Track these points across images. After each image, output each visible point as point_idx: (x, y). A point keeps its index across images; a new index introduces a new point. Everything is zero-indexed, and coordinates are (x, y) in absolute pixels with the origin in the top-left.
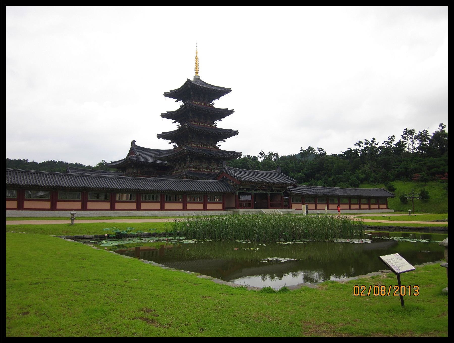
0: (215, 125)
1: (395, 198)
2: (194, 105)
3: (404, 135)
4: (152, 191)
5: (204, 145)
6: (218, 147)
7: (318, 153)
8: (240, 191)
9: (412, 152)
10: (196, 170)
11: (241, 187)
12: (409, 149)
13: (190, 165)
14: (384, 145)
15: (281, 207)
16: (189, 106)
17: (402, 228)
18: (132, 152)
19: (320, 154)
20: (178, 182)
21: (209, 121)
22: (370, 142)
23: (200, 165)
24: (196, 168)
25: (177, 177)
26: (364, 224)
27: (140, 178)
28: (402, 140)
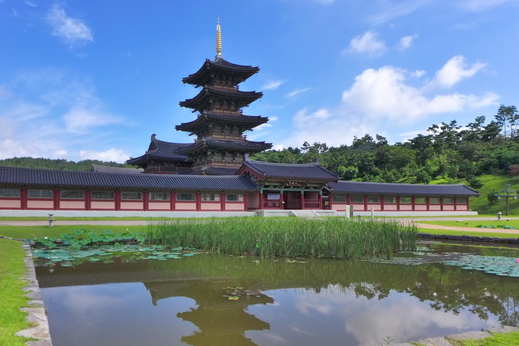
1: (480, 197)
3: (499, 114)
5: (236, 136)
7: (377, 142)
8: (266, 189)
9: (510, 137)
10: (218, 164)
11: (267, 184)
12: (505, 132)
14: (468, 129)
15: (319, 207)
17: (482, 239)
18: (152, 146)
19: (380, 143)
21: (233, 108)
22: (449, 126)
23: (223, 159)
24: (219, 162)
26: (420, 231)
28: (496, 121)
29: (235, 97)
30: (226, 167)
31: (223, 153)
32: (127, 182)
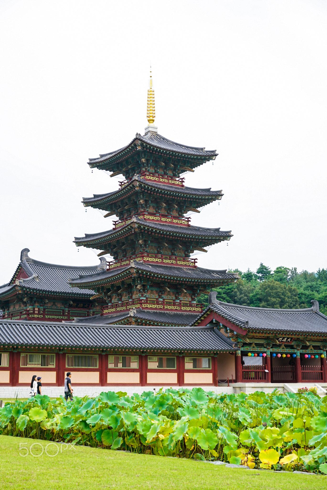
0: (187, 220)
2: (147, 182)
4: (86, 349)
5: (166, 259)
6: (192, 262)
10: (154, 306)
11: (248, 341)
13: (141, 298)
16: (140, 186)
20: (24, 327)
21: (175, 214)
23: (177, 298)
25: (116, 322)
27: (54, 323)
29: (180, 197)
30: (166, 312)
31: (177, 289)
32: (137, 339)
